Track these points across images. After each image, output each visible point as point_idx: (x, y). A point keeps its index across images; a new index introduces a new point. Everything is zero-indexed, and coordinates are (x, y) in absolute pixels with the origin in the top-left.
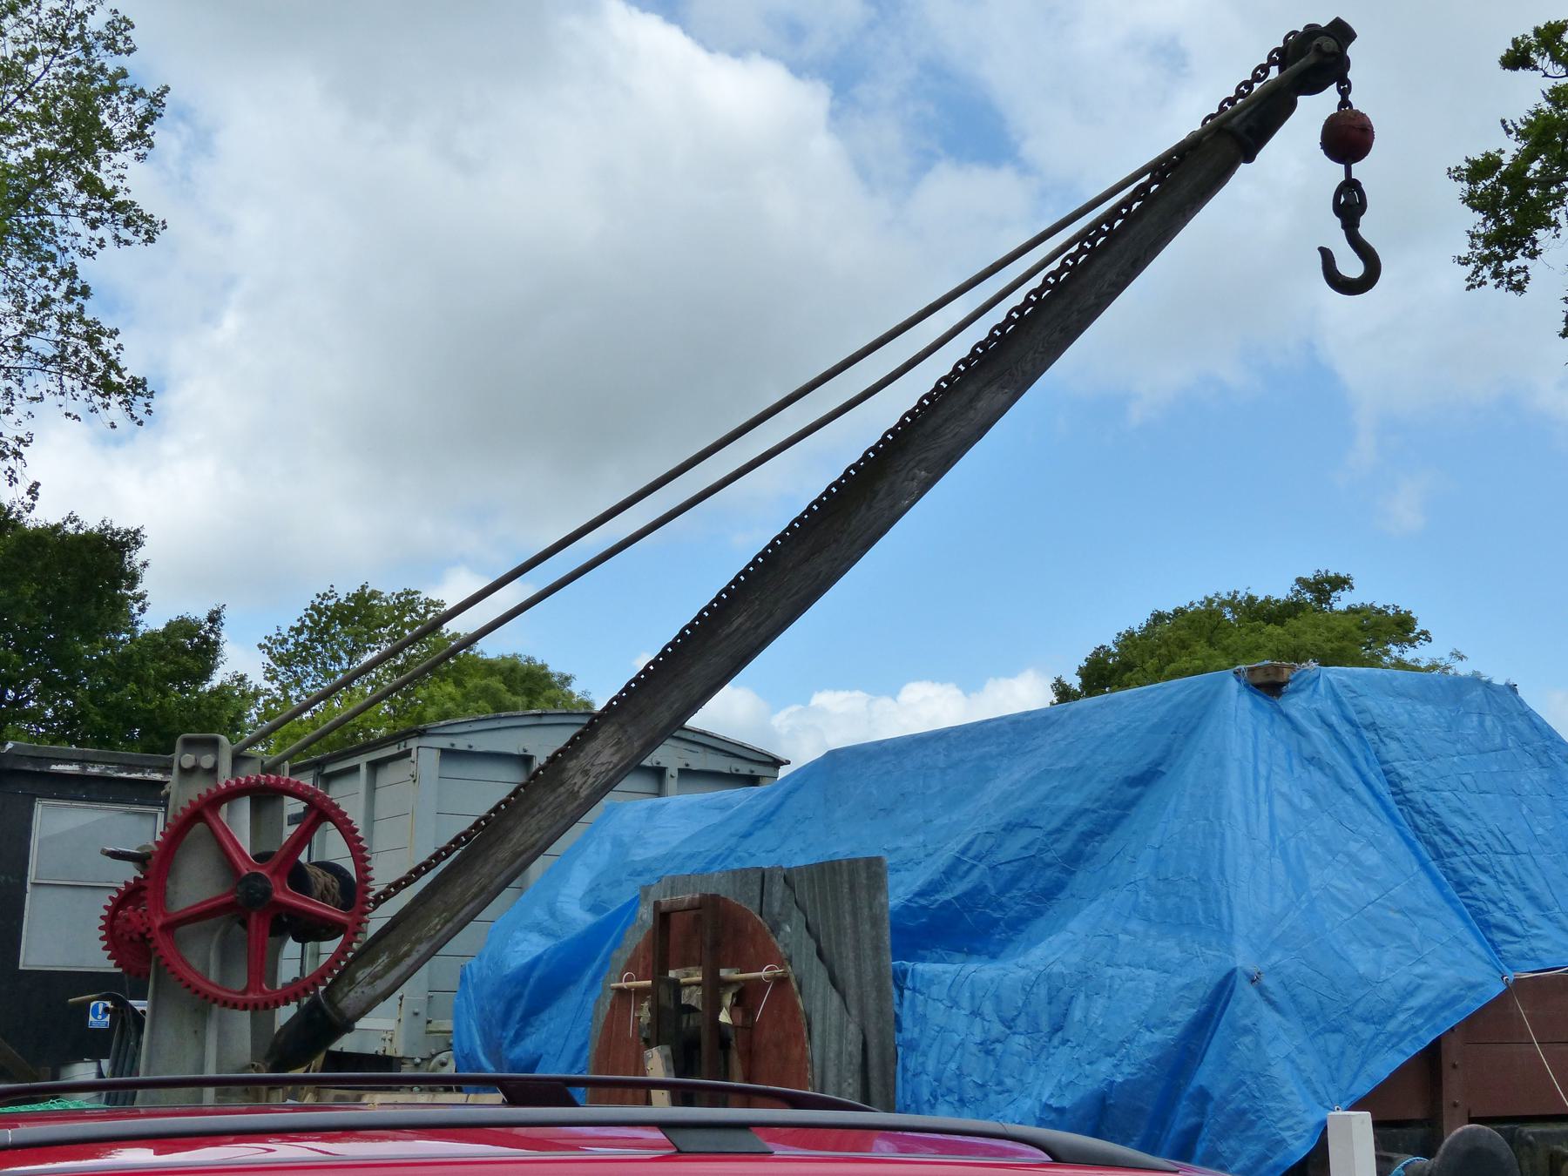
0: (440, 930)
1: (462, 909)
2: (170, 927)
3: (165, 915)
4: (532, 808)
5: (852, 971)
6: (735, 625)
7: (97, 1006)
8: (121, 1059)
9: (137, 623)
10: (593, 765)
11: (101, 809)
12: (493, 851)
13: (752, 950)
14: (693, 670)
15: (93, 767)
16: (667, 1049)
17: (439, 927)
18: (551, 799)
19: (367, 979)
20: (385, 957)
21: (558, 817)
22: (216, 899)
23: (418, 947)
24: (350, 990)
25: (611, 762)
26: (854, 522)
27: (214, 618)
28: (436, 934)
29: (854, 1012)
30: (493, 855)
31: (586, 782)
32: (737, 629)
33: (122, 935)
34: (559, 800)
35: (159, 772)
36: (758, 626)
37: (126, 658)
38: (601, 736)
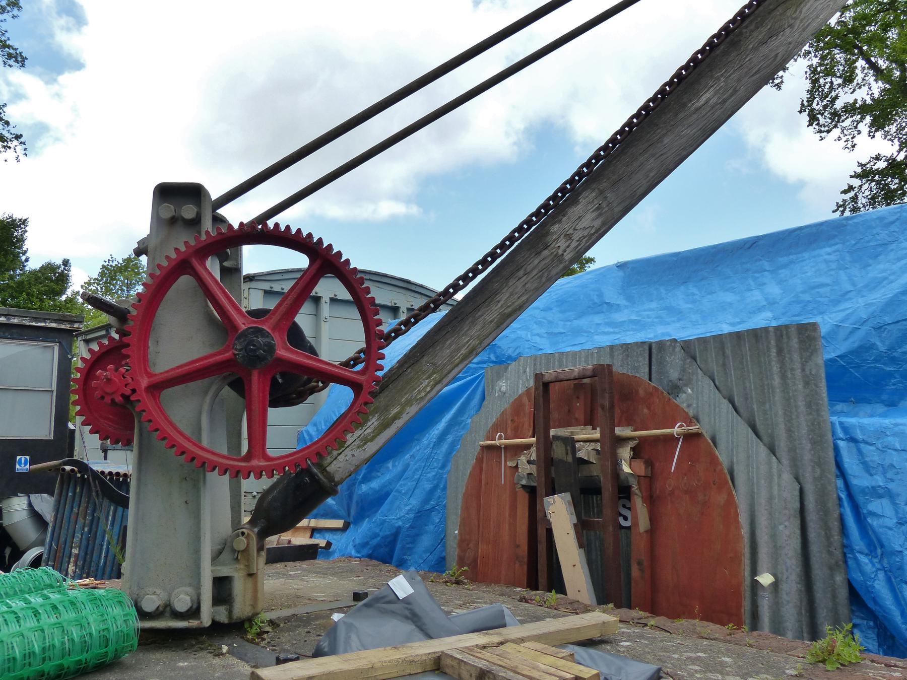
0: (429, 392)
1: (453, 369)
2: (158, 387)
3: (150, 375)
4: (518, 270)
5: (782, 426)
6: (703, 99)
7: (21, 459)
8: (61, 506)
9: (25, 266)
10: (575, 229)
11: (20, 344)
12: (480, 313)
13: (646, 411)
14: (666, 140)
15: (14, 319)
16: (567, 496)
17: (428, 389)
18: (536, 262)
19: (357, 443)
20: (374, 420)
21: (544, 279)
22: (206, 358)
23: (408, 409)
24: (340, 454)
25: (593, 227)
26: (804, 10)
27: (66, 263)
28: (426, 395)
29: (785, 462)
30: (480, 317)
31: (568, 246)
32: (706, 102)
33: (102, 398)
34: (543, 263)
35: (55, 322)
36: (724, 101)
37: (21, 283)
38: (583, 201)
